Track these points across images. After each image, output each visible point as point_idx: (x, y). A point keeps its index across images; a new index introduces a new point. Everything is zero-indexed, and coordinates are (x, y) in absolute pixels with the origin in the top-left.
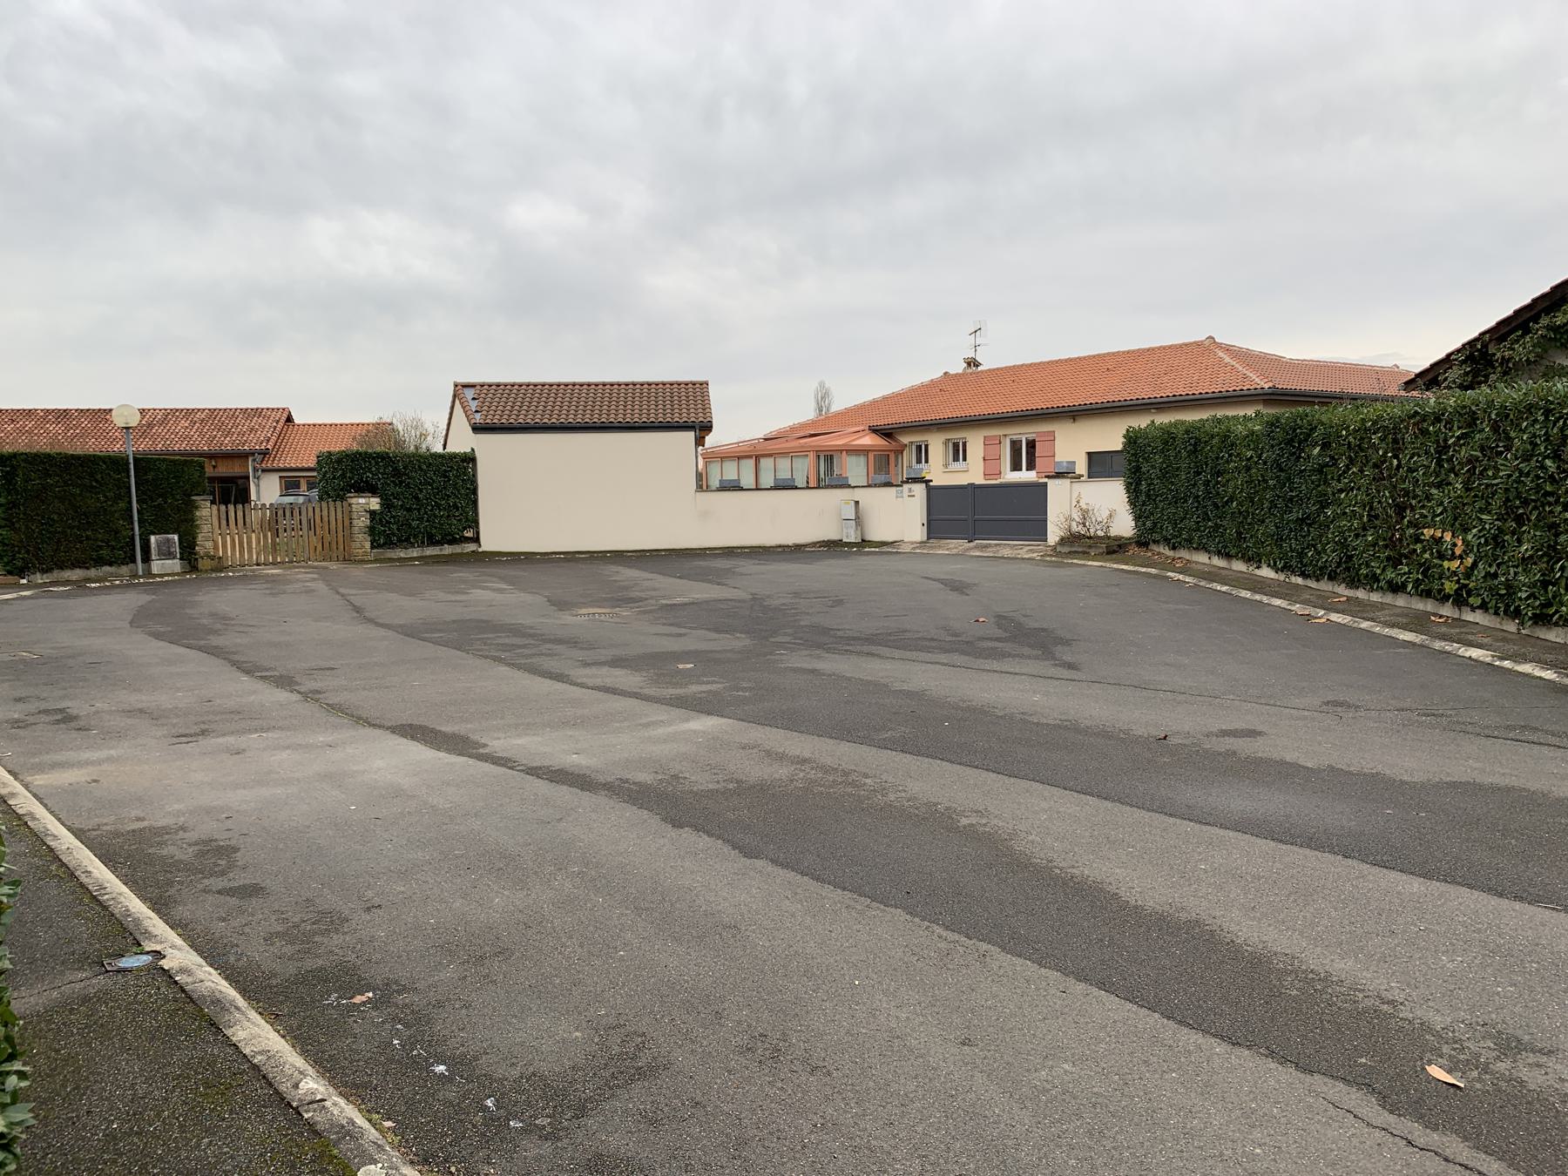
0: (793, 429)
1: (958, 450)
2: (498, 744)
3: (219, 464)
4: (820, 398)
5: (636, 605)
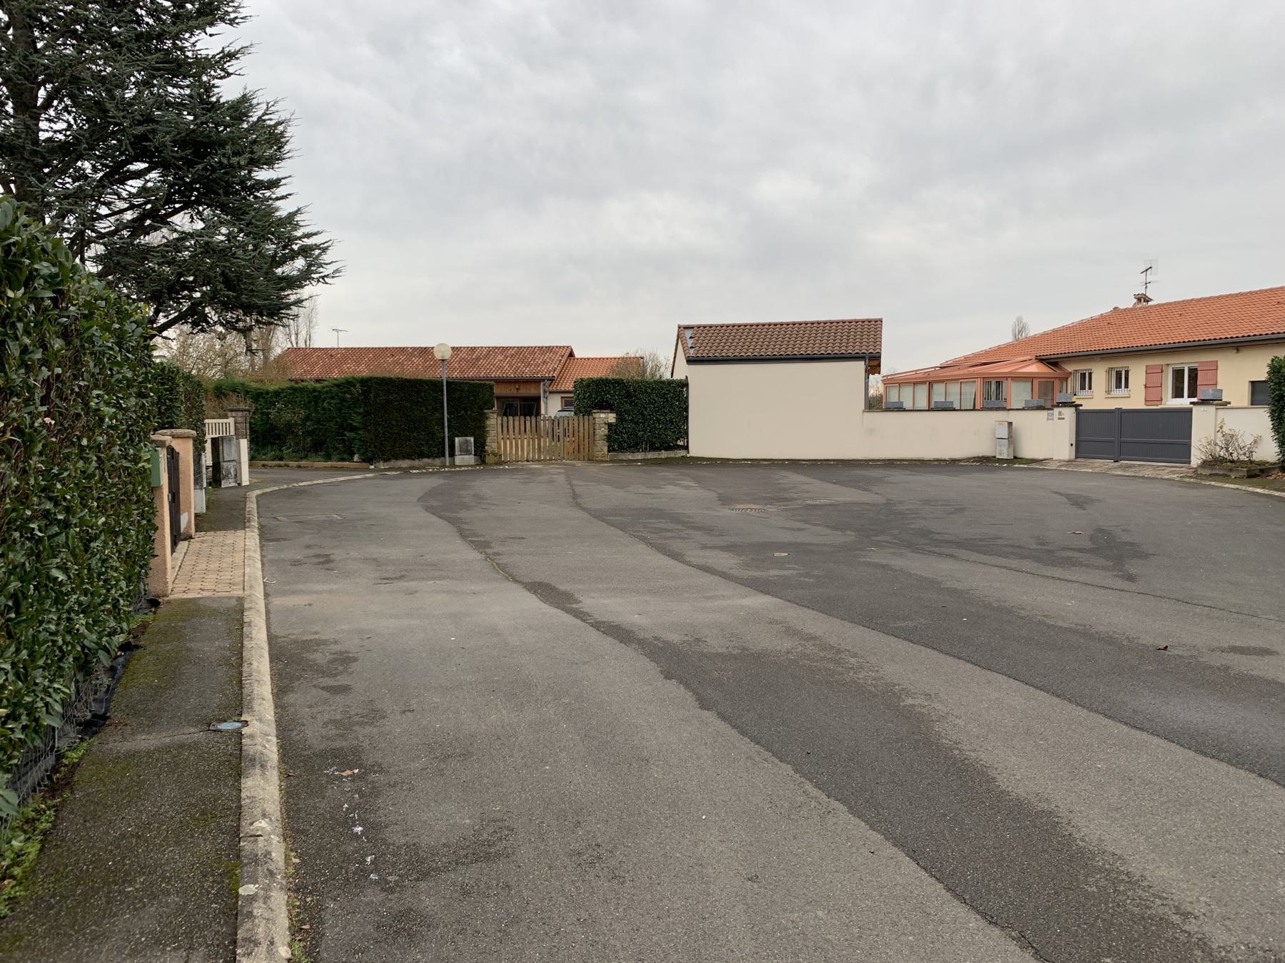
0: (967, 358)
1: (1121, 378)
2: (589, 602)
3: (521, 387)
4: (1017, 332)
5: (785, 503)
